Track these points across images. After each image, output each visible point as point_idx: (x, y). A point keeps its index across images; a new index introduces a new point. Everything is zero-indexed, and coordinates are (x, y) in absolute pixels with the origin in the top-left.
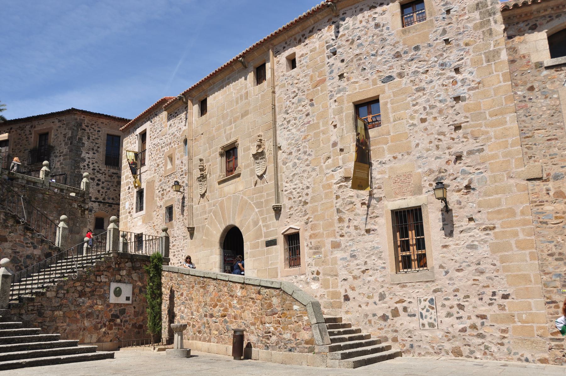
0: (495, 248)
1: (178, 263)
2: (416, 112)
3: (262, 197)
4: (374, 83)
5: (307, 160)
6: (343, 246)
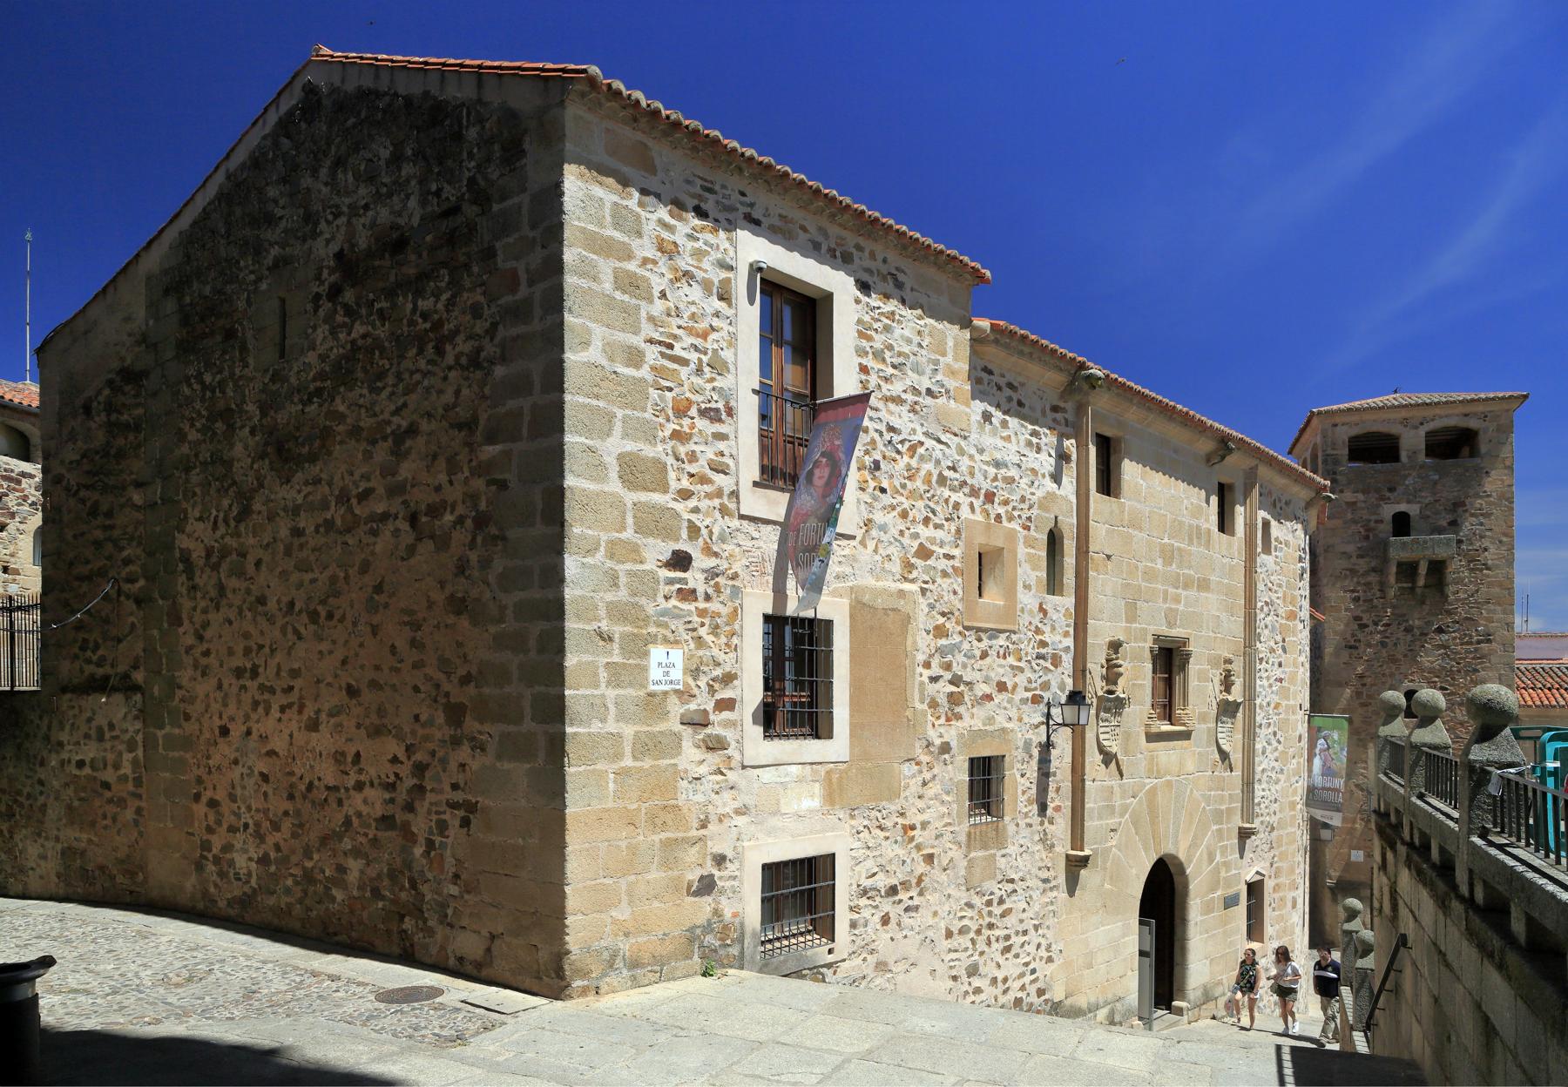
1: (1022, 975)
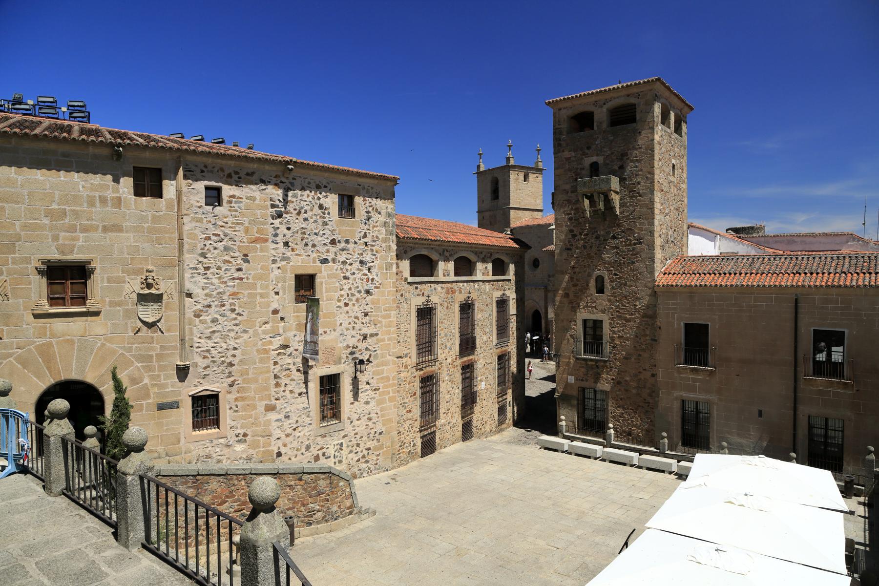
0: (379, 402)
2: (342, 296)
3: (151, 349)
4: (314, 262)
5: (235, 319)
6: (278, 409)
